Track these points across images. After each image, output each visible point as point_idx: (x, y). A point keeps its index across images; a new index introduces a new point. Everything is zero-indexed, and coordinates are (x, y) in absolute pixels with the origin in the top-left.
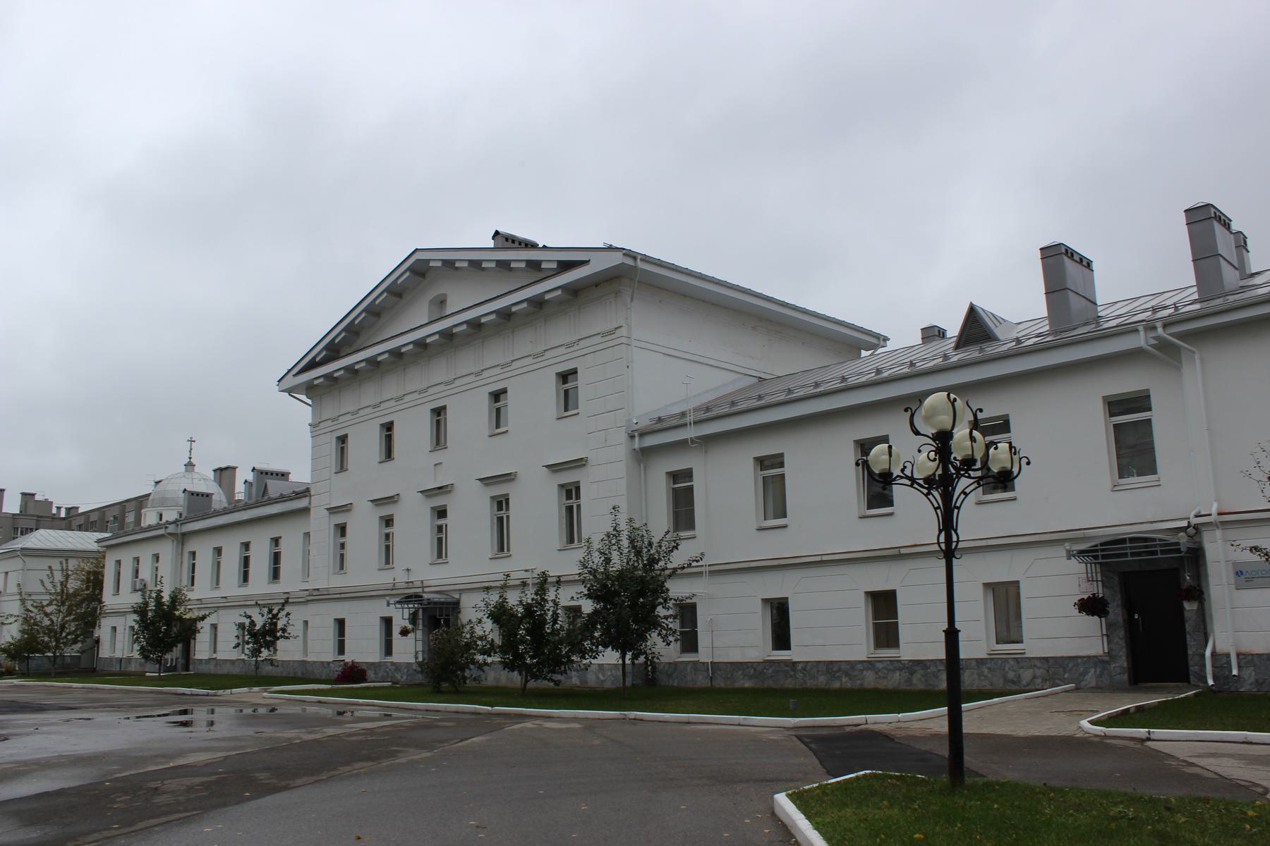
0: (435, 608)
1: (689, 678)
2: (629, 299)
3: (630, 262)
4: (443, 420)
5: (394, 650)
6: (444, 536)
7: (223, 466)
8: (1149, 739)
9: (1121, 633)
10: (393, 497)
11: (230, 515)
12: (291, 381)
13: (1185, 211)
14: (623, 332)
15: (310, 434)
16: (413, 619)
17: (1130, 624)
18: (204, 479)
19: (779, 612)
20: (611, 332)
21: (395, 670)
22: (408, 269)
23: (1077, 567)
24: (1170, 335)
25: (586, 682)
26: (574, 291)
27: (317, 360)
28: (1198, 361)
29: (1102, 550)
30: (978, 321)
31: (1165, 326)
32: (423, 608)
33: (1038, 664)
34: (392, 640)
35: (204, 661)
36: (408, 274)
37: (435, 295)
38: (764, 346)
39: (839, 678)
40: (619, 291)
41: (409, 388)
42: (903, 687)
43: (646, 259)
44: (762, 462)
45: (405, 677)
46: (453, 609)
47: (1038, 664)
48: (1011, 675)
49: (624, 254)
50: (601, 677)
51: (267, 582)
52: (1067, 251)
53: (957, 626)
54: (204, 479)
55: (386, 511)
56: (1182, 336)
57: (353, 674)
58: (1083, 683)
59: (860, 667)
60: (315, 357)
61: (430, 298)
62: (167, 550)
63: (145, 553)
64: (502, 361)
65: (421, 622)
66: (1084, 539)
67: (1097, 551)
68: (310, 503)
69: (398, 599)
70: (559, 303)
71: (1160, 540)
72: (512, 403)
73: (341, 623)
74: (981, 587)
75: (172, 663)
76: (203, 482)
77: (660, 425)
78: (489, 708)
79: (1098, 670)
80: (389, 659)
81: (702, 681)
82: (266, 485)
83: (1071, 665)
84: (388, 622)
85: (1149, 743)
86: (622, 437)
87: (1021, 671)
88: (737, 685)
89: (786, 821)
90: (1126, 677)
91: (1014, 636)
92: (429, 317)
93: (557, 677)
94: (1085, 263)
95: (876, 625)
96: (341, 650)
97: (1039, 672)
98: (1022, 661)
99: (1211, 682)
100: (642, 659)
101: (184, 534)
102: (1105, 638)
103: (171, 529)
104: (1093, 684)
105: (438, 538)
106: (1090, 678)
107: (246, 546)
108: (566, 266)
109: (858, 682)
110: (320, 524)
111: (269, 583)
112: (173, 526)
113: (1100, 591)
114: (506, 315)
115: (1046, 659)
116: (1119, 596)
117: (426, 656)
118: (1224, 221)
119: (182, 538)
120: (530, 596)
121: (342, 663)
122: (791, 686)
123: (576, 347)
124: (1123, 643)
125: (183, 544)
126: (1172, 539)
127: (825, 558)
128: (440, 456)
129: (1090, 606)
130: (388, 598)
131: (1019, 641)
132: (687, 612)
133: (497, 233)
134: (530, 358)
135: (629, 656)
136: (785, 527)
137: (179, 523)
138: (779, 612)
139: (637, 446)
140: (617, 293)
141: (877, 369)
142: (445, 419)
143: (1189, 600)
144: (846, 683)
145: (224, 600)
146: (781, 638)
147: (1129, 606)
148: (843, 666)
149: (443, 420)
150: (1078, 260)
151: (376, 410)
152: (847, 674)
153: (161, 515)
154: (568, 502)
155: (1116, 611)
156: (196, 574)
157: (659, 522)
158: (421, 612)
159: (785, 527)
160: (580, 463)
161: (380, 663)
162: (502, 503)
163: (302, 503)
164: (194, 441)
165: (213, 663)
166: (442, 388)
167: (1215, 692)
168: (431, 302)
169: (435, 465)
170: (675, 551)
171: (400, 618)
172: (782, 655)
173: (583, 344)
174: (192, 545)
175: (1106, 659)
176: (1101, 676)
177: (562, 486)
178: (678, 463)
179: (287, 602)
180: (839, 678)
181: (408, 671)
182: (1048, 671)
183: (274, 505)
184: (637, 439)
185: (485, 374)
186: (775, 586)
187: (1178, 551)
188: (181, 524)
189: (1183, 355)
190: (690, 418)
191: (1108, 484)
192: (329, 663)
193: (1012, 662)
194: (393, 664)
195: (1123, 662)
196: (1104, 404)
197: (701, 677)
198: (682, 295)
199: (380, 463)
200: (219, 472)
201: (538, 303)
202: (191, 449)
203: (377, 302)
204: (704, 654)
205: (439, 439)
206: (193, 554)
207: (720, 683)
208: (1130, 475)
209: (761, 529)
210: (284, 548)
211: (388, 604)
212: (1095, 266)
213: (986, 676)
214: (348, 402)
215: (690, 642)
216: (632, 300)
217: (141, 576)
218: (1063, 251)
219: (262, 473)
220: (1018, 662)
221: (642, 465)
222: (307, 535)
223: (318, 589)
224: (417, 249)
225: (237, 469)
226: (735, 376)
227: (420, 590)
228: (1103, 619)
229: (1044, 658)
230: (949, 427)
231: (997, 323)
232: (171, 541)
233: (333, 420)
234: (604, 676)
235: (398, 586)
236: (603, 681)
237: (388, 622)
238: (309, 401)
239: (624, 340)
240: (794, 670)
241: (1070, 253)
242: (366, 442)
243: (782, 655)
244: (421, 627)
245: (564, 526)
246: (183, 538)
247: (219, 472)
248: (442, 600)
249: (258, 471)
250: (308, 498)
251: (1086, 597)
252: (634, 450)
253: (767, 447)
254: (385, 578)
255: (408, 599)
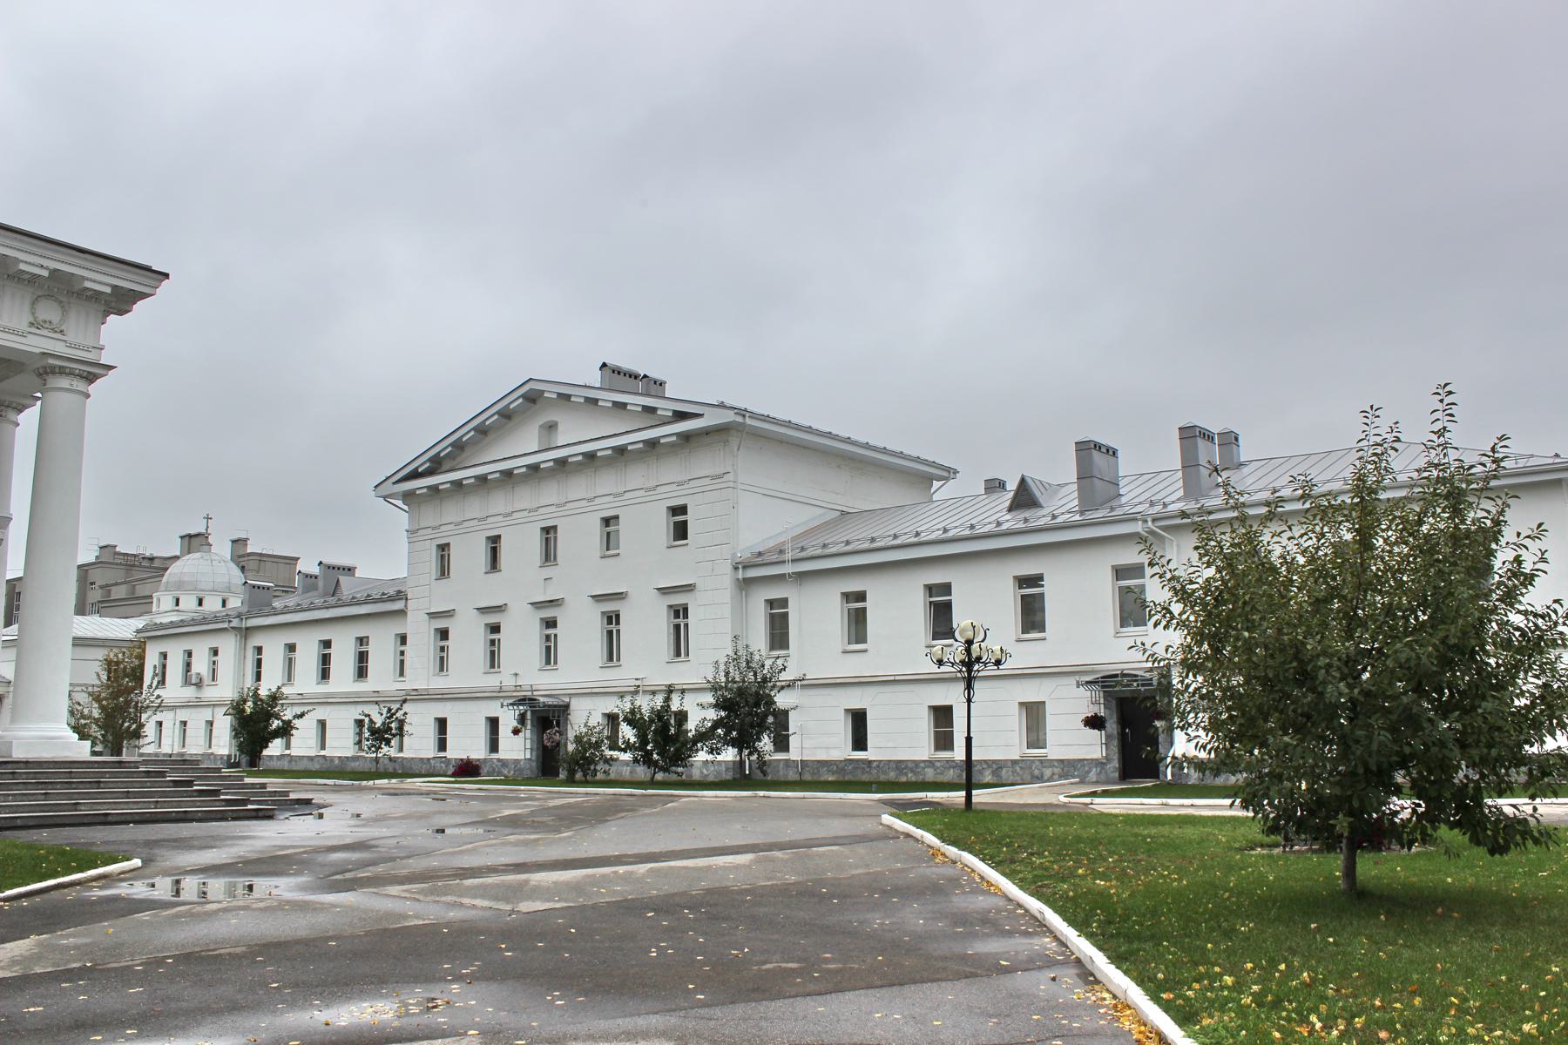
0: (549, 710)
1: (781, 773)
2: (736, 449)
3: (740, 419)
4: (552, 539)
5: (404, 748)
6: (553, 645)
7: (193, 532)
8: (1092, 804)
9: (1115, 742)
10: (501, 606)
11: (312, 612)
12: (389, 488)
13: (1179, 428)
14: (730, 477)
15: (406, 539)
16: (522, 719)
17: (1123, 737)
18: (224, 561)
19: (859, 719)
20: (719, 477)
21: (502, 766)
22: (522, 396)
23: (1085, 693)
24: (1156, 527)
25: (691, 776)
26: (686, 437)
27: (420, 470)
28: (1175, 548)
29: (1102, 682)
30: (1027, 490)
31: (1154, 520)
32: (532, 711)
33: (1056, 764)
34: (498, 739)
35: (275, 758)
36: (521, 400)
37: (547, 420)
38: (847, 482)
39: (906, 774)
40: (728, 441)
41: (518, 506)
42: (955, 781)
43: (754, 416)
44: (847, 597)
45: (512, 772)
46: (564, 711)
47: (1056, 764)
48: (1036, 772)
49: (735, 413)
50: (705, 772)
51: (352, 680)
52: (1095, 446)
53: (972, 735)
54: (224, 561)
55: (492, 619)
56: (1165, 529)
57: (467, 769)
58: (1087, 779)
59: (922, 765)
60: (417, 468)
61: (541, 423)
62: (228, 646)
63: (201, 649)
64: (614, 491)
65: (529, 722)
66: (1092, 672)
67: (1098, 682)
68: (406, 606)
69: (511, 701)
70: (672, 445)
71: (1142, 676)
72: (624, 528)
73: (442, 724)
74: (1017, 705)
75: (235, 760)
76: (222, 564)
77: (758, 560)
78: (644, 791)
79: (1099, 769)
80: (494, 756)
81: (792, 776)
82: (338, 581)
83: (1079, 766)
84: (493, 723)
85: (1091, 806)
86: (729, 568)
87: (1044, 769)
88: (822, 779)
89: (1030, 508)
90: (1117, 774)
91: (1041, 745)
92: (539, 446)
93: (680, 770)
94: (1111, 453)
95: (936, 733)
96: (442, 745)
97: (1056, 770)
98: (1044, 762)
99: (1169, 777)
100: (754, 757)
101: (247, 629)
102: (1104, 746)
103: (235, 623)
104: (1094, 780)
105: (491, 651)
106: (1093, 776)
107: (327, 644)
108: (681, 416)
109: (921, 777)
110: (419, 629)
111: (354, 682)
112: (237, 620)
113: (1102, 710)
114: (621, 451)
115: (1062, 761)
116: (1115, 716)
117: (534, 753)
118: (1208, 435)
119: (246, 633)
120: (659, 701)
121: (444, 759)
122: (867, 780)
123: (686, 486)
124: (1116, 750)
125: (246, 639)
126: (1148, 675)
127: (897, 678)
128: (549, 572)
129: (1094, 722)
130: (502, 700)
131: (1044, 747)
132: (782, 717)
133: (604, 365)
134: (643, 491)
135: (746, 752)
136: (865, 651)
137: (244, 617)
138: (859, 719)
139: (740, 577)
140: (726, 442)
141: (945, 528)
142: (555, 538)
143: (1158, 720)
144: (911, 777)
145: (300, 697)
146: (860, 742)
147: (1123, 722)
148: (910, 765)
149: (552, 539)
150: (1105, 451)
151: (481, 523)
152: (912, 771)
153: (178, 600)
154: (676, 620)
155: (1112, 726)
156: (263, 669)
157: (758, 640)
158: (529, 714)
159: (865, 651)
160: (689, 588)
161: (485, 759)
162: (613, 618)
163: (399, 605)
164: (211, 519)
165: (287, 759)
166: (553, 509)
167: (1171, 784)
168: (540, 426)
169: (545, 579)
170: (783, 672)
171: (508, 719)
172: (860, 755)
173: (692, 484)
174: (256, 641)
175: (1105, 761)
176: (1100, 773)
177: (670, 607)
178: (776, 593)
179: (405, 701)
180: (906, 774)
181: (516, 766)
182: (1063, 770)
183: (363, 606)
184: (741, 570)
185: (598, 501)
186: (856, 699)
187: (1151, 685)
188: (246, 619)
189: (1166, 543)
190: (788, 556)
191: (1112, 632)
192: (429, 759)
193: (1037, 763)
194: (499, 760)
195: (1115, 764)
196: (1112, 571)
197: (791, 773)
198: (779, 441)
199: (486, 573)
200: (187, 539)
201: (652, 444)
202: (208, 527)
203: (487, 423)
204: (794, 754)
205: (549, 555)
206: (259, 650)
207: (807, 777)
208: (1129, 625)
209: (845, 652)
210: (372, 649)
211: (502, 706)
212: (1119, 454)
213: (1018, 773)
214: (451, 512)
215: (782, 744)
216: (738, 449)
217: (195, 669)
218: (1092, 446)
219: (329, 568)
220: (1042, 763)
221: (744, 593)
222: (403, 639)
223: (416, 690)
224: (531, 379)
225: (299, 561)
226: (823, 510)
227: (530, 693)
228: (1103, 732)
229: (1060, 760)
230: (972, 637)
231: (1043, 489)
232: (234, 636)
233: (434, 528)
234: (707, 771)
235: (504, 689)
236: (707, 776)
237: (493, 723)
238: (406, 508)
239: (731, 484)
240: (870, 767)
241: (1098, 447)
242: (469, 555)
243: (860, 755)
244: (529, 727)
245: (672, 641)
246: (246, 633)
247: (187, 539)
248: (555, 703)
249: (325, 565)
250: (404, 601)
251: (1090, 715)
252: (738, 579)
253: (853, 585)
254: (492, 681)
255: (522, 701)
